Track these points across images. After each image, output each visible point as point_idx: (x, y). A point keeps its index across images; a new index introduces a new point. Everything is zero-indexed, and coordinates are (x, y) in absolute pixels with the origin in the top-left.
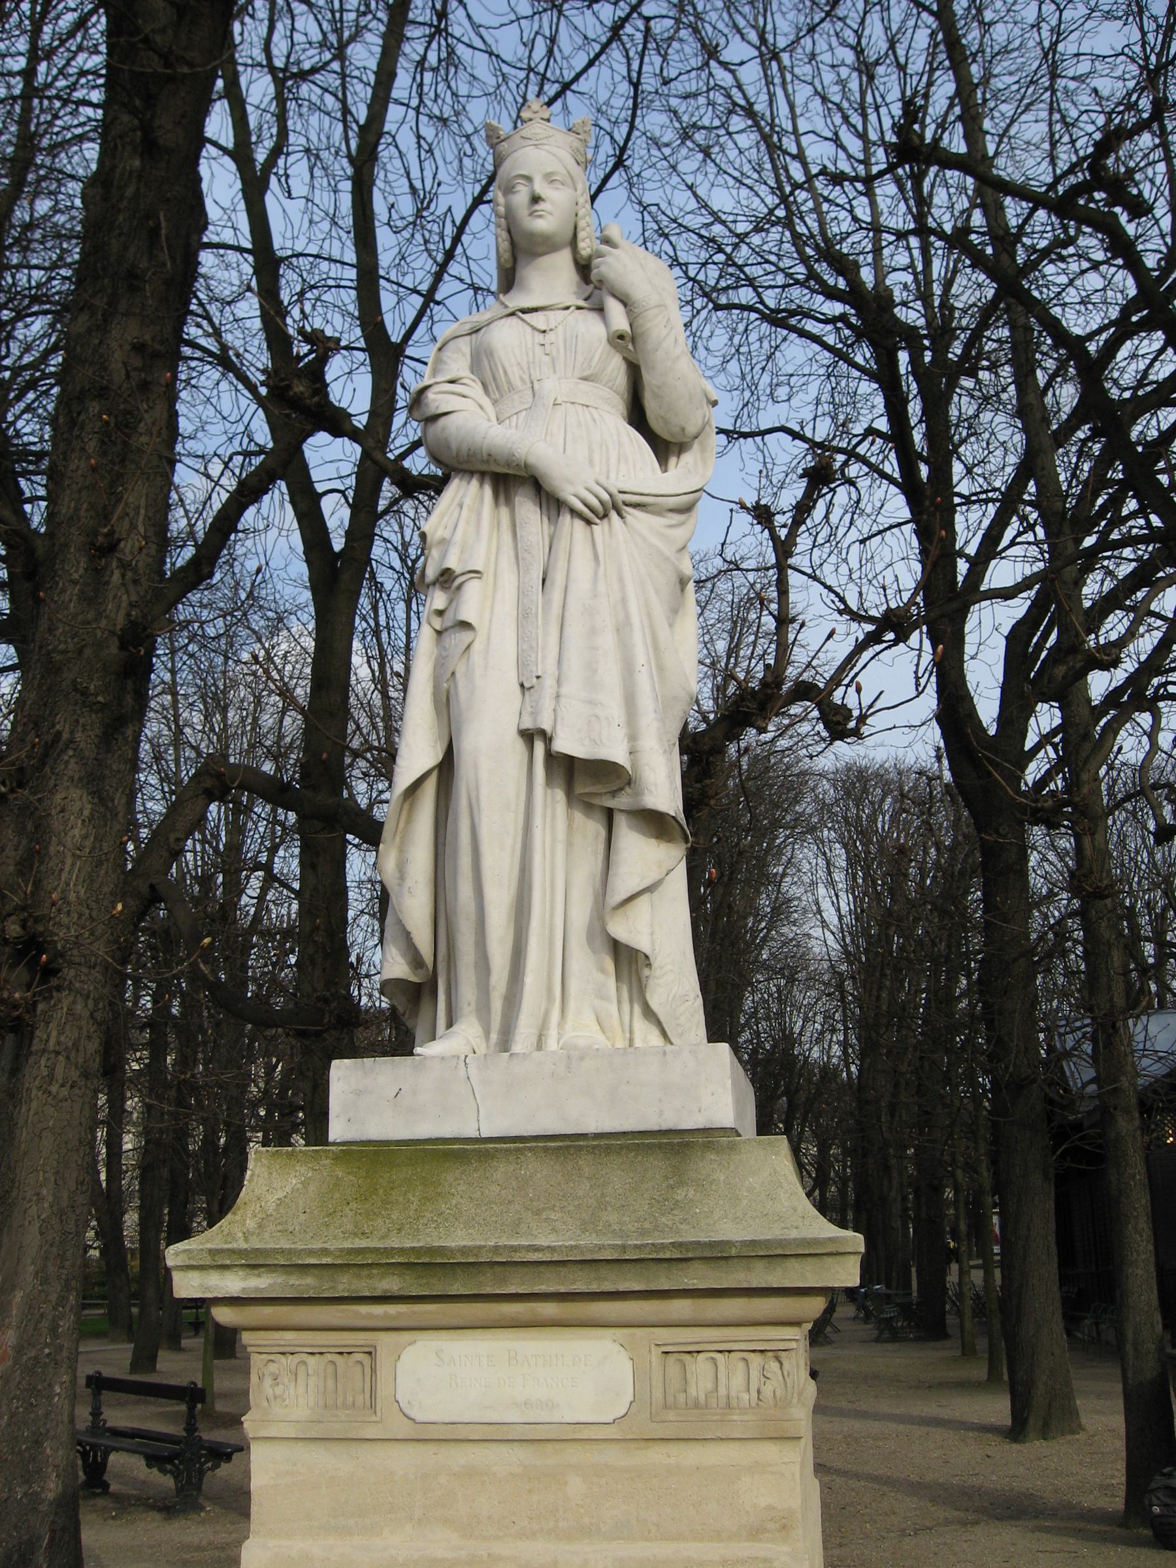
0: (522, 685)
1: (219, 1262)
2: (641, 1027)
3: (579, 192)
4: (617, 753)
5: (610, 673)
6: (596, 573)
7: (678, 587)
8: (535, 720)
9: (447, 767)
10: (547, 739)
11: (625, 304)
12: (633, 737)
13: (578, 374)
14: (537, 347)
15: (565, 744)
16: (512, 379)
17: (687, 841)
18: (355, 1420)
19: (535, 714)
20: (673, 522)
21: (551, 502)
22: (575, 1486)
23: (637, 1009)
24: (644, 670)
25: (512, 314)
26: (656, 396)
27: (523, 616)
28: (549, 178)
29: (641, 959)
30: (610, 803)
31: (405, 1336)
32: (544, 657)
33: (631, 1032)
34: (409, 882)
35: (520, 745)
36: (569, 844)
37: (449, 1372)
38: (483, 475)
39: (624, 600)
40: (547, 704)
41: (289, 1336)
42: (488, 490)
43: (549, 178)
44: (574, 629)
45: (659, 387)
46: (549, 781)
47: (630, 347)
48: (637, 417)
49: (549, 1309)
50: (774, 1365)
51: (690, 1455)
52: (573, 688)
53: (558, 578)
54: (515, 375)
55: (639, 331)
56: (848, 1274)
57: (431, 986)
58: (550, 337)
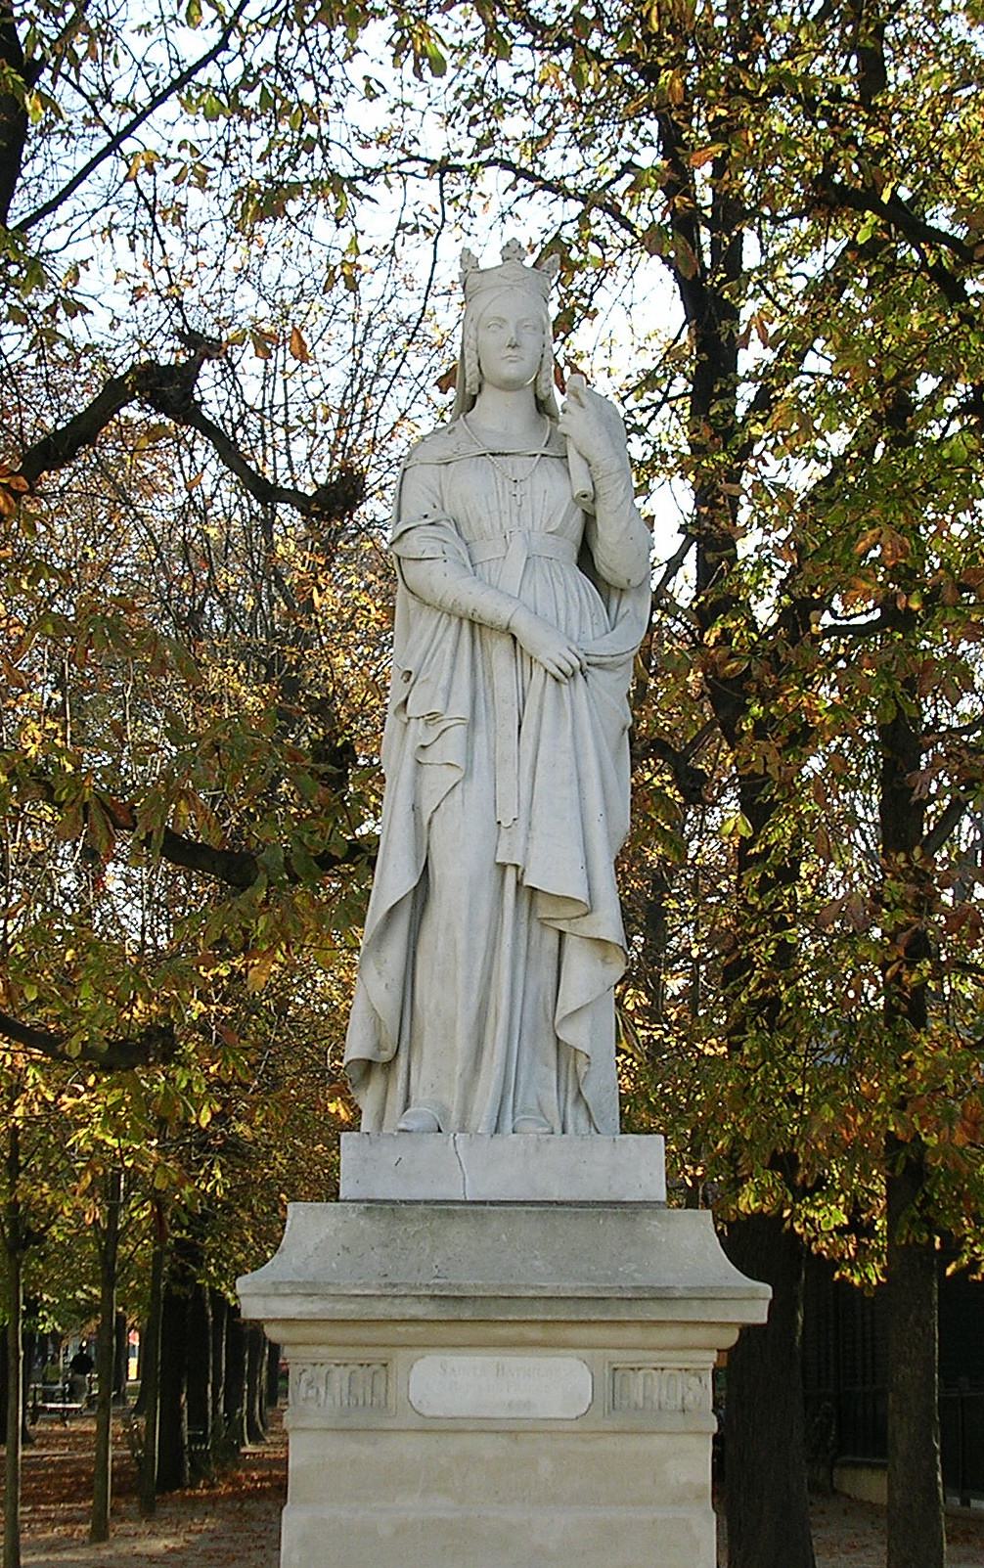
1: (276, 1291)
9: (422, 892)
18: (370, 1415)
22: (545, 1466)
31: (418, 1352)
37: (448, 1381)
41: (323, 1350)
48: (585, 558)
49: (534, 1333)
50: (694, 1381)
51: (635, 1444)
56: (759, 1314)
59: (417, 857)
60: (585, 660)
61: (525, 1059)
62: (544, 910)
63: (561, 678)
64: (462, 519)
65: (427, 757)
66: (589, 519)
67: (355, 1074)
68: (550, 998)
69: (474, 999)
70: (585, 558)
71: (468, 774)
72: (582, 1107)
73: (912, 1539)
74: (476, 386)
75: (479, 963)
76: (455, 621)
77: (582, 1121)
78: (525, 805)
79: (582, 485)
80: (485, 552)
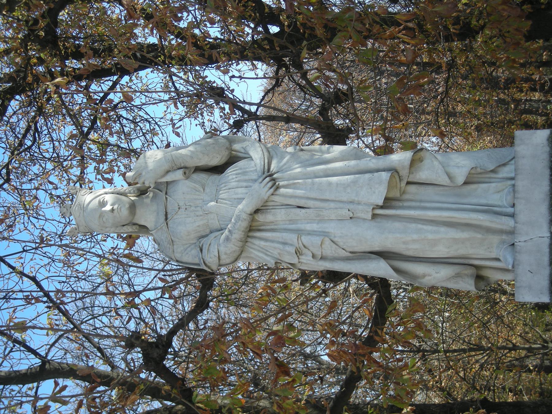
36: (421, 201)
59: (370, 258)
61: (474, 201)
62: (395, 193)
63: (275, 186)
64: (199, 234)
65: (318, 253)
66: (199, 169)
67: (482, 285)
68: (441, 188)
69: (443, 229)
70: (219, 170)
71: (325, 234)
72: (500, 169)
73: (322, 6)
74: (134, 227)
75: (425, 227)
76: (249, 240)
77: (507, 169)
78: (341, 205)
79: (179, 175)
80: (216, 224)
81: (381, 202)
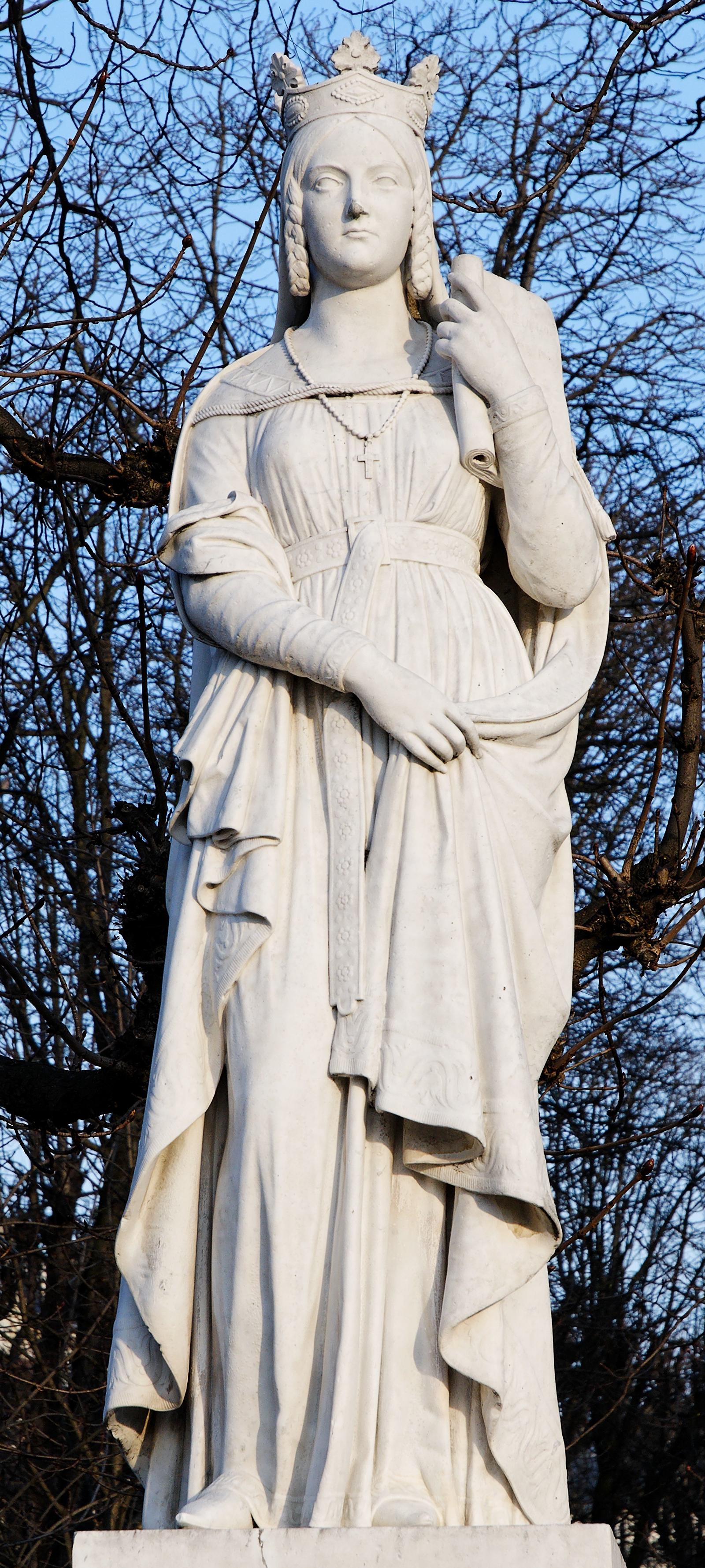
0: (335, 1008)
2: (486, 1487)
3: (418, 191)
4: (466, 1119)
5: (460, 1001)
6: (442, 849)
7: (551, 849)
8: (354, 1062)
10: (372, 1092)
11: (488, 405)
12: (490, 1091)
13: (413, 514)
14: (356, 467)
15: (391, 1102)
16: (316, 517)
17: (556, 1234)
19: (355, 1055)
20: (547, 752)
21: (381, 737)
23: (479, 1460)
24: (505, 995)
25: (315, 397)
26: (524, 543)
27: (336, 907)
28: (375, 174)
29: (486, 1398)
30: (448, 1174)
32: (368, 972)
33: (468, 1495)
34: (161, 1274)
35: (333, 1092)
38: (275, 674)
39: (479, 887)
40: (372, 1042)
42: (284, 694)
43: (375, 174)
44: (408, 932)
45: (532, 536)
46: (369, 1135)
47: (492, 469)
48: (495, 567)
52: (408, 1015)
53: (388, 853)
54: (320, 507)
55: (505, 448)
57: (180, 1418)
58: (374, 447)
60: (476, 731)
79: (480, 438)
81: (388, 1103)
